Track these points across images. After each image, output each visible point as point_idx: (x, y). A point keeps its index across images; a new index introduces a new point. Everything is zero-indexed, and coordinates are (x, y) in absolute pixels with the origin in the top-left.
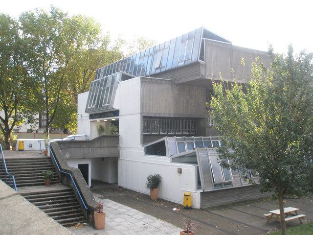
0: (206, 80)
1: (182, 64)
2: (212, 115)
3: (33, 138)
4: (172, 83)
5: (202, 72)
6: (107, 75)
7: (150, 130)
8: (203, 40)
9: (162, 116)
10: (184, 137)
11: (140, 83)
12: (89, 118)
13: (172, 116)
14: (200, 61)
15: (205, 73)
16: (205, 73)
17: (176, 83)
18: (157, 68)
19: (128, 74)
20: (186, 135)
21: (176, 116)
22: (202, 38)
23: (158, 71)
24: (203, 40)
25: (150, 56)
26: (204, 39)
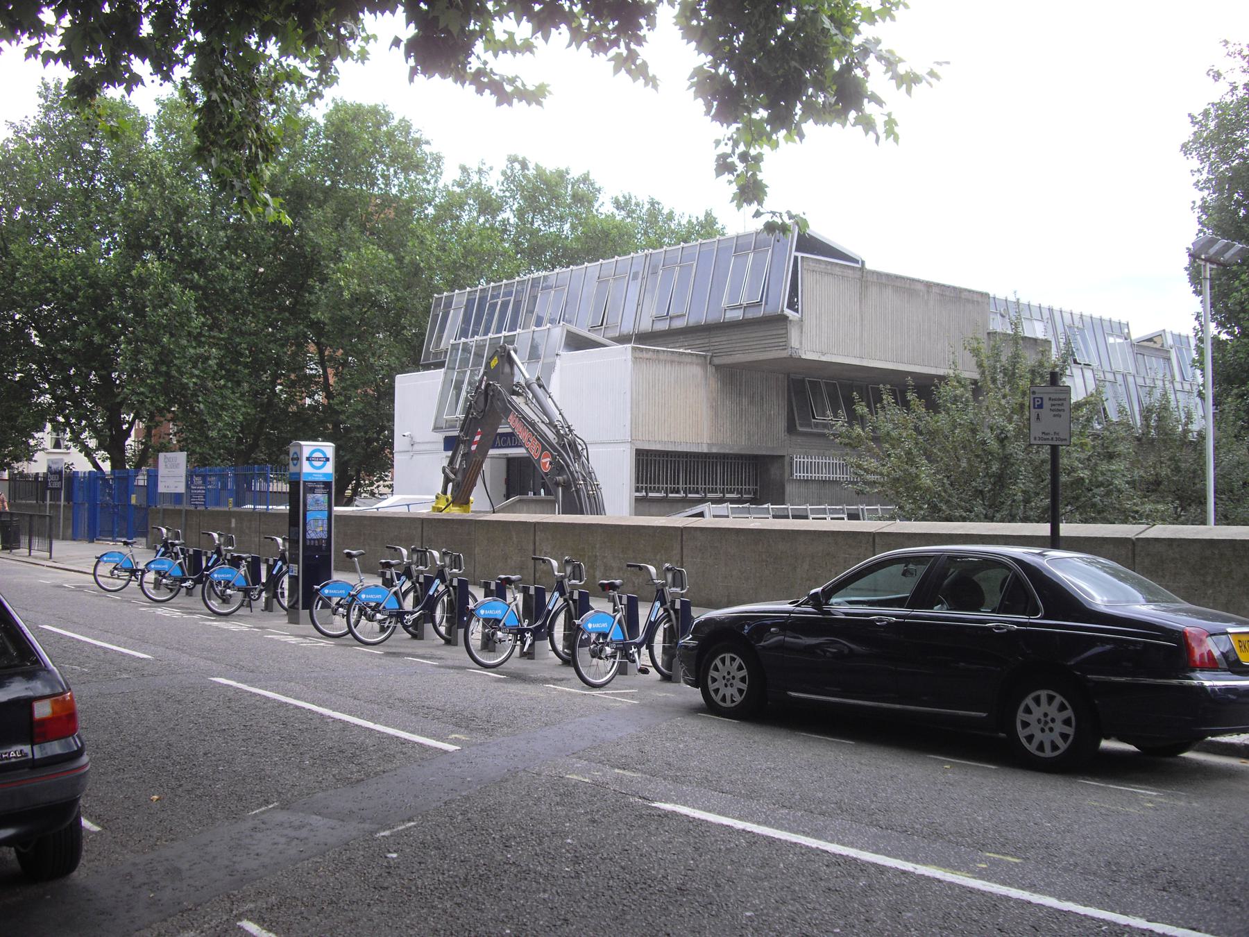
0: (800, 359)
1: (738, 315)
2: (1138, 473)
3: (1215, 487)
4: (708, 361)
5: (794, 339)
6: (513, 327)
7: (681, 486)
8: (796, 258)
9: (679, 449)
10: (747, 505)
11: (630, 364)
12: (442, 446)
13: (705, 450)
14: (788, 312)
15: (801, 343)
16: (801, 343)
17: (717, 361)
18: (659, 318)
19: (584, 332)
20: (732, 501)
21: (714, 450)
22: (794, 253)
23: (662, 326)
24: (796, 258)
25: (635, 277)
26: (799, 255)
